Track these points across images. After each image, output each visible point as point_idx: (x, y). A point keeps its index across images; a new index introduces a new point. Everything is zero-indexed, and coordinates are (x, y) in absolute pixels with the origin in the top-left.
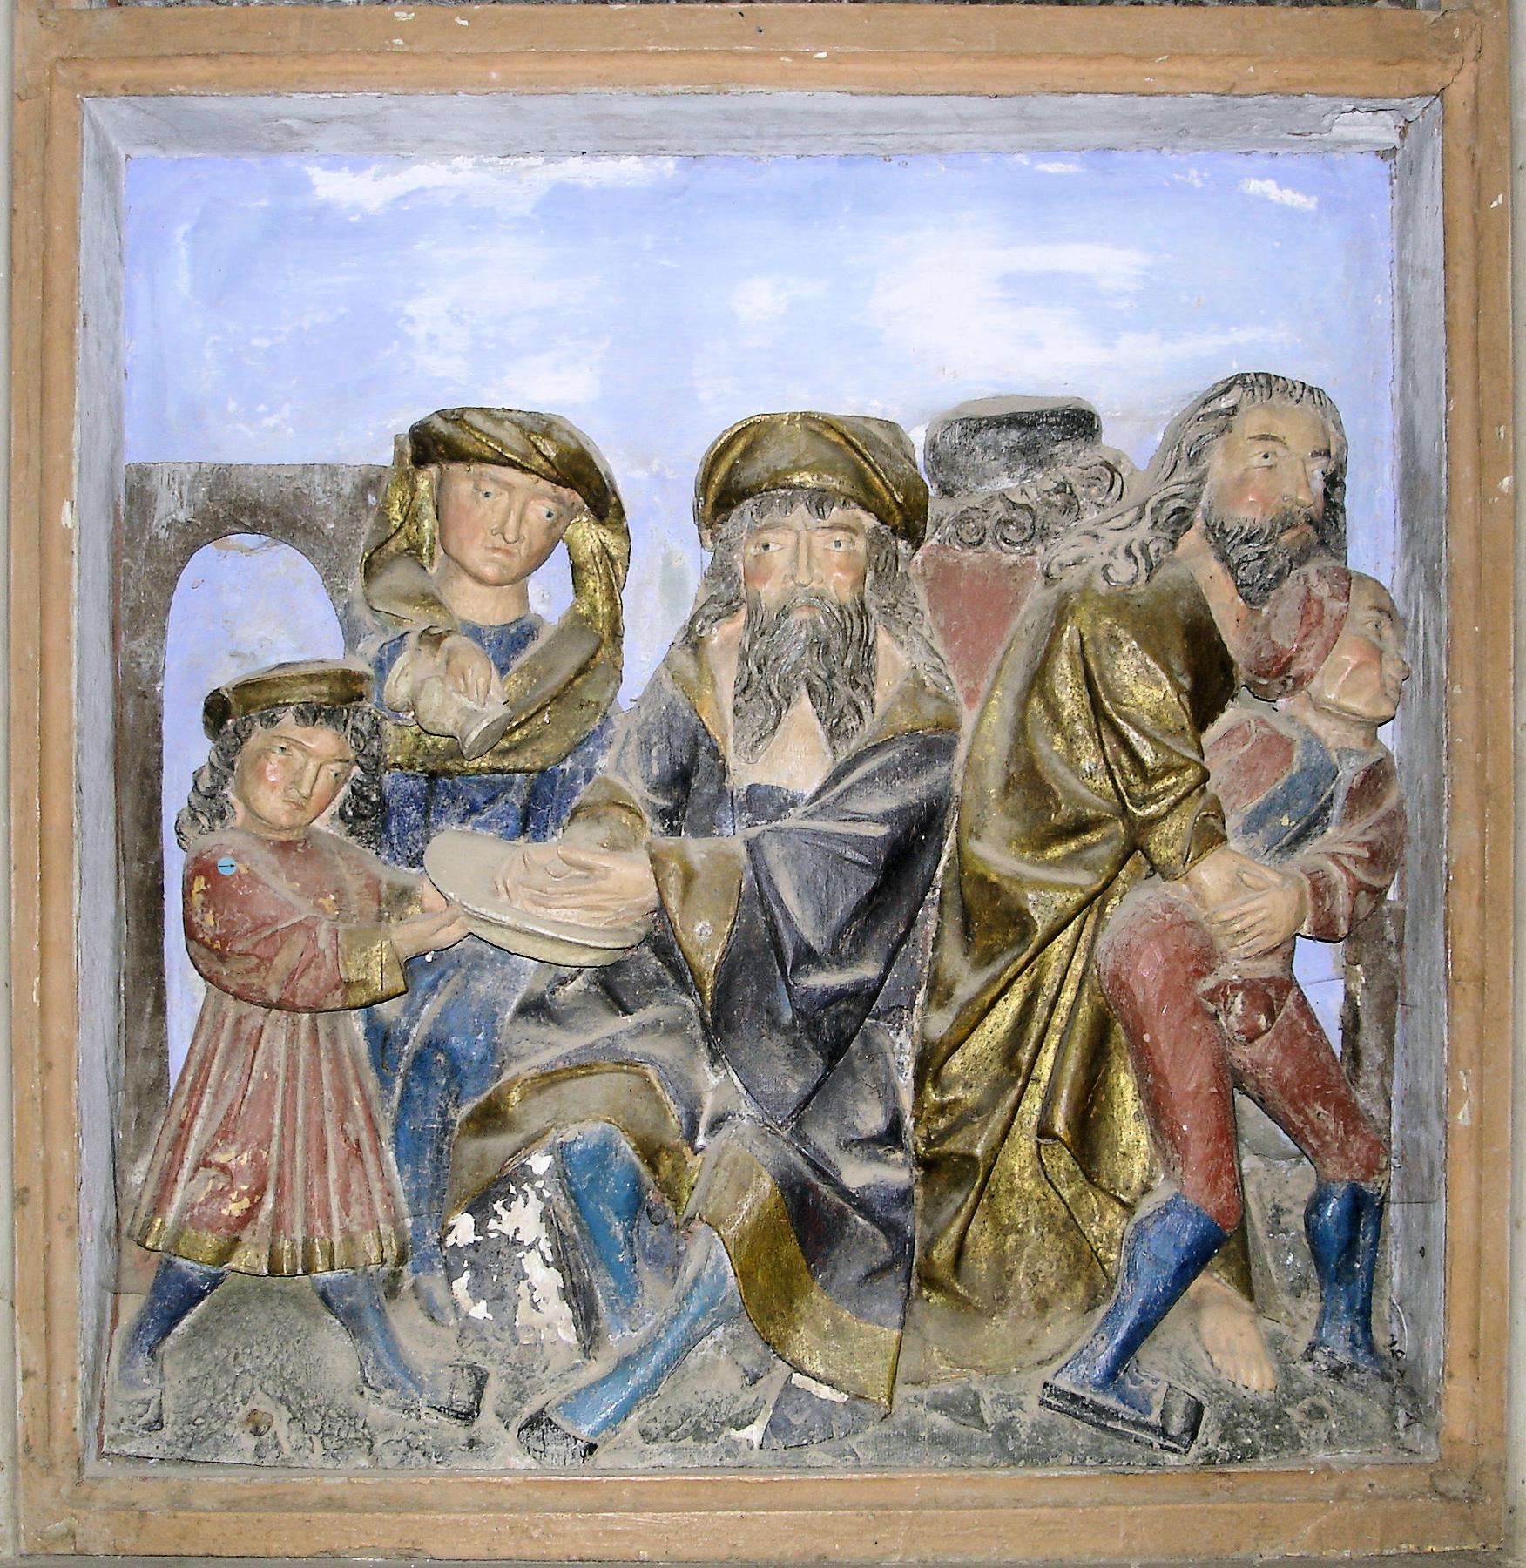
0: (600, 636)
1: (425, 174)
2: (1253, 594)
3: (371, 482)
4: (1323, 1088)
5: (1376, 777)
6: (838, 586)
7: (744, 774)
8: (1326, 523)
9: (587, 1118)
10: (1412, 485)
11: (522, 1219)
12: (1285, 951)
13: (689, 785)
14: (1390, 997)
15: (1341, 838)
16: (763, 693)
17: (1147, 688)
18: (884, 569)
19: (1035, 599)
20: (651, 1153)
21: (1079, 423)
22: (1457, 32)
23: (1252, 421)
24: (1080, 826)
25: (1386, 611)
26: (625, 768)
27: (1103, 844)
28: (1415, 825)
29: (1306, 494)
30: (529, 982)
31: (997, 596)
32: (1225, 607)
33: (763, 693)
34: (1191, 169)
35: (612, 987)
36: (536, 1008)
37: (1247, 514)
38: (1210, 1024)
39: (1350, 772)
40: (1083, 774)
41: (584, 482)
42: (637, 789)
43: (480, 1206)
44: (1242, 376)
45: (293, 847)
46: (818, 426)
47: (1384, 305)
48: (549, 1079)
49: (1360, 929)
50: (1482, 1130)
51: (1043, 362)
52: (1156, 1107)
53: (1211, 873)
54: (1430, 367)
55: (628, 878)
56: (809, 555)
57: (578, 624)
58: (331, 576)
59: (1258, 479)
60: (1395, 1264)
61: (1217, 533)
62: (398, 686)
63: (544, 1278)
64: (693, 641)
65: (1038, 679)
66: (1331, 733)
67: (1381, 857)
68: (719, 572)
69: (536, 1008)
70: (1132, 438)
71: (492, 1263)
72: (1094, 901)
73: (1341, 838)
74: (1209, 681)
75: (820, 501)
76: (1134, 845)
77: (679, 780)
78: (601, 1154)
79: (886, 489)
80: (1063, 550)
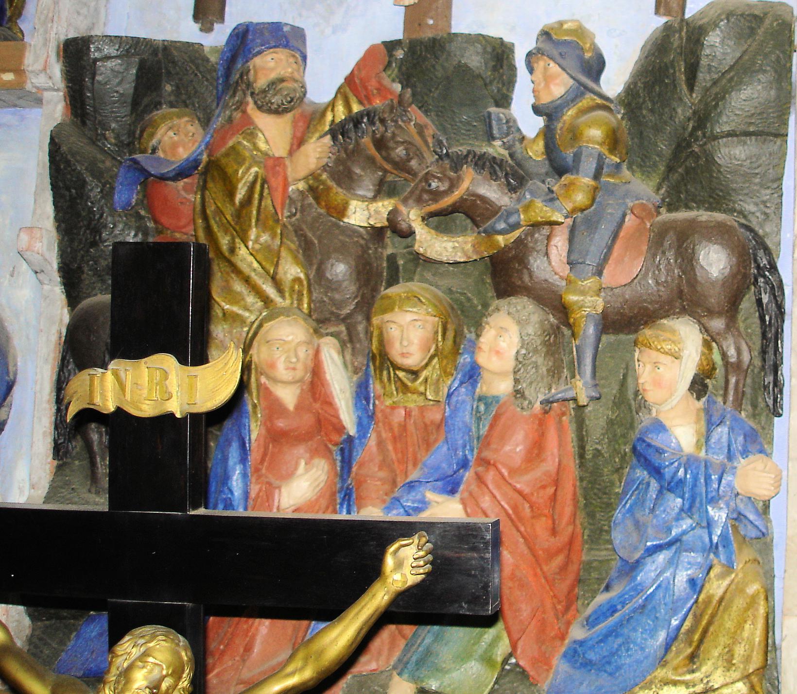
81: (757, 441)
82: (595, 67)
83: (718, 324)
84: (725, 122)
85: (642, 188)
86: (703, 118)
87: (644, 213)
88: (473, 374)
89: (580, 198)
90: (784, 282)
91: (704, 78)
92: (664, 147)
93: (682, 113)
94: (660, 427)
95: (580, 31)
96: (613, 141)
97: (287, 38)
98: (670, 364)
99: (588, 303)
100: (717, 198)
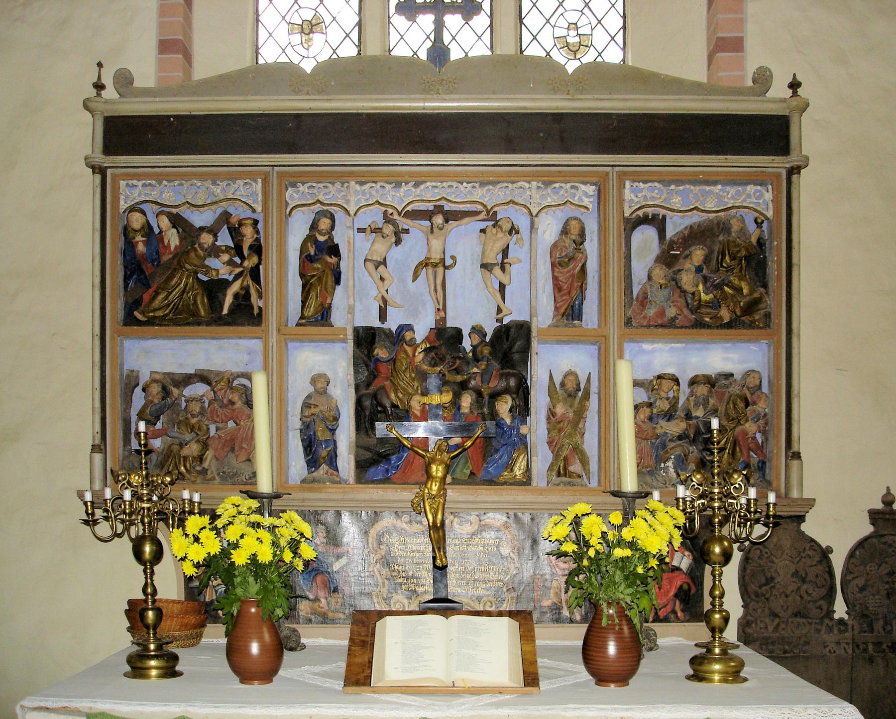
0: (676, 399)
1: (656, 345)
2: (752, 394)
3: (652, 381)
4: (760, 449)
5: (765, 415)
6: (706, 393)
7: (694, 415)
8: (760, 387)
9: (678, 451)
10: (769, 382)
11: (670, 464)
12: (755, 434)
13: (688, 416)
14: (767, 439)
15: (761, 422)
16: (696, 405)
17: (741, 405)
18: (710, 392)
19: (727, 395)
20: (685, 455)
21: (732, 375)
22: (758, 133)
23: (752, 375)
24: (733, 420)
25: (766, 396)
26: (680, 413)
27: (736, 421)
28: (770, 420)
29: (758, 383)
30: (670, 437)
31: (723, 394)
32: (748, 396)
33: (696, 405)
34: (744, 345)
35: (680, 438)
36: (670, 440)
37: (751, 385)
38: (661, 596)
39: (762, 414)
40: (732, 413)
41: (677, 381)
42: (683, 415)
43: (665, 463)
44: (420, 264)
45: (644, 422)
46: (704, 376)
47: (766, 361)
48: (673, 448)
49: (764, 433)
50: (777, 453)
51: (728, 367)
52: (741, 451)
53: (747, 425)
54: (772, 370)
55: (683, 425)
56: (702, 390)
57: (674, 397)
58: (647, 391)
59: (752, 382)
60: (767, 471)
61: (748, 388)
62: (657, 404)
63: (672, 470)
64: (688, 399)
65: (728, 403)
66: (760, 410)
67: (766, 424)
68: (692, 391)
69: (670, 440)
70: (738, 377)
71: (666, 469)
72: (734, 428)
73: (761, 422)
74: (747, 404)
75: (705, 384)
76: (739, 422)
77: (687, 415)
78: (680, 455)
79: (710, 381)
80: (730, 389)
81: (524, 422)
82: (485, 335)
83: (514, 396)
84: (514, 350)
85: (496, 365)
86: (511, 348)
87: (498, 371)
88: (459, 409)
89: (483, 367)
90: (581, 655)
91: (510, 339)
92: (500, 355)
93: (505, 347)
94: (503, 419)
95: (481, 327)
96: (490, 354)
97: (410, 328)
98: (504, 407)
99: (486, 392)
100: (513, 367)
